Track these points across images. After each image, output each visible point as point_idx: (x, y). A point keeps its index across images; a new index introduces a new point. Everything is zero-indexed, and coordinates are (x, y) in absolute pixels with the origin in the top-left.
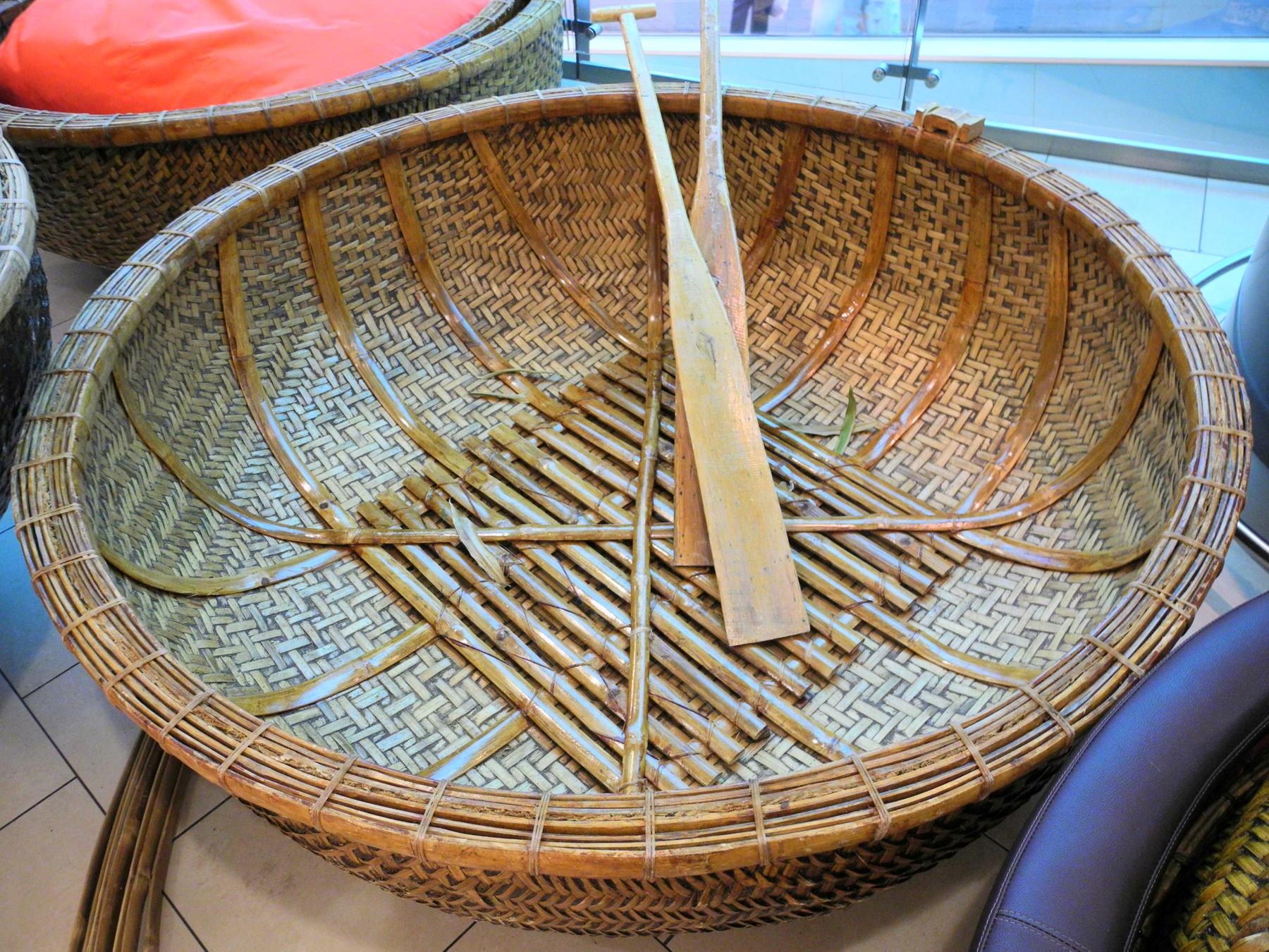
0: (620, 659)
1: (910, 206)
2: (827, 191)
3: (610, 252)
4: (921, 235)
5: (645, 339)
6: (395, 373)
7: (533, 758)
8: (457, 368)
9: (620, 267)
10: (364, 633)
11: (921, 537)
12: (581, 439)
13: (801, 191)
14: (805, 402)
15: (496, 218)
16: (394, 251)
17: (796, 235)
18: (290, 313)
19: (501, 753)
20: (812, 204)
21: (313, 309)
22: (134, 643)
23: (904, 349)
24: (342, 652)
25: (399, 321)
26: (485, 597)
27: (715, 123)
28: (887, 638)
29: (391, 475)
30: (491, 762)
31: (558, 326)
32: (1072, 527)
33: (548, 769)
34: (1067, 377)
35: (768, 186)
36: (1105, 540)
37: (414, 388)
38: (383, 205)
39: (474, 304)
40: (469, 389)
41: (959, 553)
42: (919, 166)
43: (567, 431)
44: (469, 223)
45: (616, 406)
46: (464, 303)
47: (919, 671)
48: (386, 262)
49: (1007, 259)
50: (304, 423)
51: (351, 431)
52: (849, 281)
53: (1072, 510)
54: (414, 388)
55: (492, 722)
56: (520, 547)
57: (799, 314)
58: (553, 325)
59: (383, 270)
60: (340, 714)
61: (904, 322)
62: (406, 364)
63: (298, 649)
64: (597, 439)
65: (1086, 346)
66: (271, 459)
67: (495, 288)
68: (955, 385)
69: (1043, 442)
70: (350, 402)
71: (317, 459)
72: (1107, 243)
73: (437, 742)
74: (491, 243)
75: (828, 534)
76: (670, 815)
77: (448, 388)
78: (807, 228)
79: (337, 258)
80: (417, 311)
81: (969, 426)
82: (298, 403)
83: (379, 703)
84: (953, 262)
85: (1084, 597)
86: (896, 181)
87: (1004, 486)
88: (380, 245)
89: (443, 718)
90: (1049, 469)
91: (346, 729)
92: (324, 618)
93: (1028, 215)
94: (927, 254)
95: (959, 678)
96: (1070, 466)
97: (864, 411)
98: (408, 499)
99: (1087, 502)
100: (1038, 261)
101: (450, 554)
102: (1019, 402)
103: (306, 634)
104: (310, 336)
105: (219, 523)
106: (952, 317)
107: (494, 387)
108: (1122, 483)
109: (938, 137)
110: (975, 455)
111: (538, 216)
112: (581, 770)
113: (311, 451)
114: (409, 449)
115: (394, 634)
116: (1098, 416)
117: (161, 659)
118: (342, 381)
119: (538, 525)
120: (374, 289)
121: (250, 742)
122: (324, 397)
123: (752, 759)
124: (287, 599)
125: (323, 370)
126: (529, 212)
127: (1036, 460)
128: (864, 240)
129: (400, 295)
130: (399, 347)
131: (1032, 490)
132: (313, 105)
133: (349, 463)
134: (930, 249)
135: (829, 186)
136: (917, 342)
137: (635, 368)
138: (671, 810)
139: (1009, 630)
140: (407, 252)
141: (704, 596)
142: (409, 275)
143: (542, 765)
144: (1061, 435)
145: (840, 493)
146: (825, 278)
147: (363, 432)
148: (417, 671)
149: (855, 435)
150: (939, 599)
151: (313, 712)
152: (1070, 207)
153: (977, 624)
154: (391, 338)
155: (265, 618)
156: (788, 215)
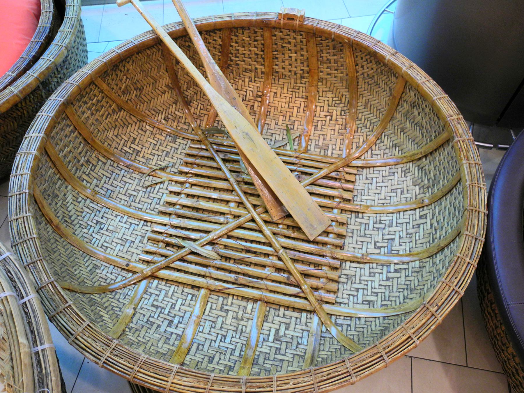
0: (280, 264)
1: (280, 47)
2: (243, 49)
3: (162, 102)
4: (287, 56)
5: (193, 132)
6: (108, 194)
8: (130, 178)
9: (168, 106)
11: (339, 170)
13: (232, 51)
14: (268, 134)
15: (112, 108)
16: (81, 143)
17: (234, 69)
18: (58, 193)
20: (238, 55)
21: (64, 186)
22: (199, 378)
24: (183, 317)
26: (216, 267)
27: (200, 40)
28: (352, 212)
31: (157, 142)
32: (387, 148)
33: (284, 315)
34: (361, 96)
35: (218, 53)
36: (402, 150)
37: (120, 196)
38: (70, 126)
40: (141, 185)
42: (281, 32)
43: (192, 185)
44: (103, 115)
45: (202, 166)
47: (368, 218)
48: (80, 149)
49: (325, 59)
50: (91, 235)
51: (110, 228)
52: (261, 80)
53: (384, 142)
54: (120, 196)
56: (216, 242)
57: (247, 99)
58: (155, 142)
59: (80, 153)
60: (204, 340)
61: (289, 90)
63: (168, 326)
64: (209, 183)
65: (367, 84)
66: (92, 258)
67: (123, 136)
68: (318, 108)
69: (361, 120)
70: (101, 215)
71: (107, 247)
72: (375, 52)
73: (242, 328)
74: (113, 120)
75: (312, 184)
76: (413, 328)
77: (133, 189)
78: (238, 65)
79: (62, 159)
80: (100, 163)
81: (331, 122)
82: (83, 229)
83: (212, 327)
84: (302, 63)
85: (405, 173)
86: (272, 39)
87: (354, 140)
88: (75, 144)
89: (236, 318)
90: (368, 130)
92: (165, 309)
93: (333, 43)
94: (290, 62)
95: (382, 215)
96: (375, 127)
97: (291, 129)
100: (339, 57)
101: (191, 258)
102: (345, 108)
103: (165, 319)
104: (70, 198)
105: (99, 297)
106: (307, 83)
107: (149, 181)
108: (399, 130)
109: (291, 22)
111: (128, 99)
112: (294, 309)
113: (102, 245)
115: (194, 299)
116: (380, 107)
117: (215, 378)
118: (92, 209)
119: (218, 230)
120: (81, 163)
121: (276, 386)
122: (90, 220)
123: (341, 274)
124: (146, 310)
125: (82, 209)
126: (124, 100)
127: (361, 128)
128: (263, 63)
129: (91, 160)
130: (103, 182)
132: (16, 95)
133: (120, 242)
134: (291, 60)
135: (244, 47)
136: (297, 96)
137: (199, 146)
138: (412, 326)
140: (85, 140)
141: (288, 226)
142: (90, 149)
143: (281, 314)
144: (367, 116)
145: (304, 166)
146: (251, 81)
147: (115, 226)
148: (214, 307)
149: (294, 140)
150: (358, 190)
152: (355, 40)
154: (98, 180)
156: (229, 62)
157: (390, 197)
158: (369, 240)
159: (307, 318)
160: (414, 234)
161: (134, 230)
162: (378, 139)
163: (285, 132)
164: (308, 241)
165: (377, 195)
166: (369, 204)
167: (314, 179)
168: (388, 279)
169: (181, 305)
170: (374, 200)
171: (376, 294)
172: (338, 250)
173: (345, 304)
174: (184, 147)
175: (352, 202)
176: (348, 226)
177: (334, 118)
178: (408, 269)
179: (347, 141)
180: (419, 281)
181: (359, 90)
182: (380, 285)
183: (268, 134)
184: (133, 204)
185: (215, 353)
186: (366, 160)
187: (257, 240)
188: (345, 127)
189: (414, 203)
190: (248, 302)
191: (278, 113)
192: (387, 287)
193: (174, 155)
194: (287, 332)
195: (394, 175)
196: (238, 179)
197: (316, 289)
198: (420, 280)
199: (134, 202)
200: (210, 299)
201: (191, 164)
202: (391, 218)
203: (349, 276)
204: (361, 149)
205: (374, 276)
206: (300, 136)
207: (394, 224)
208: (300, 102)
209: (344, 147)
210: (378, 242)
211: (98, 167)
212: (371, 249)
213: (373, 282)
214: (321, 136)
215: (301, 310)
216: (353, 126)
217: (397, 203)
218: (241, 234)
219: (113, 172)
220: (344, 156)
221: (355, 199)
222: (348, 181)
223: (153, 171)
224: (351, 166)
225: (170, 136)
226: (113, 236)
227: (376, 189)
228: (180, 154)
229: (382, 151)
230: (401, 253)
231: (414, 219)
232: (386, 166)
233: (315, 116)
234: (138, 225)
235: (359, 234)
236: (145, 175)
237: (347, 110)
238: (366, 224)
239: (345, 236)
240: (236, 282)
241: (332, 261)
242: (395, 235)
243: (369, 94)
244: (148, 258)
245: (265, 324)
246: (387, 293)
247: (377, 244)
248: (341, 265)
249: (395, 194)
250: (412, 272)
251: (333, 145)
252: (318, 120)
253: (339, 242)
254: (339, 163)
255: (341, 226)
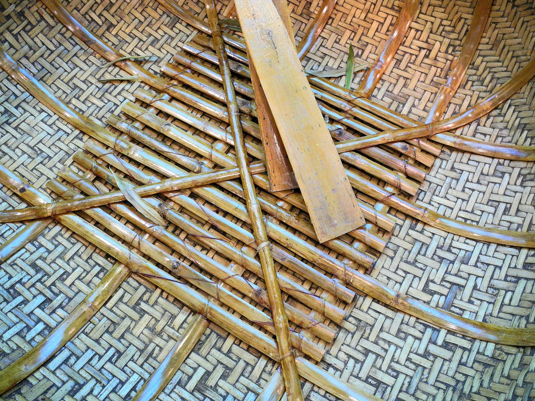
5: (206, 20)
6: (41, 74)
7: (218, 345)
10: (81, 280)
11: (411, 142)
12: (183, 103)
14: (319, 54)
19: (198, 346)
23: (376, 9)
24: (70, 299)
25: (32, 33)
28: (407, 216)
29: (62, 154)
30: (193, 355)
31: (146, 19)
32: (506, 128)
33: (230, 351)
37: (59, 83)
39: (83, 11)
40: (97, 76)
41: (436, 150)
46: (75, 12)
47: (431, 235)
51: (23, 126)
54: (59, 83)
55: (185, 325)
58: (142, 19)
60: (84, 348)
62: (48, 66)
63: (39, 307)
68: (413, 32)
69: (477, 69)
70: (15, 104)
73: (154, 349)
75: (358, 151)
77: (83, 78)
80: (43, 24)
81: (426, 61)
83: (107, 331)
87: (454, 100)
89: (152, 330)
90: (484, 88)
91: (91, 359)
92: (49, 276)
95: (456, 238)
96: (498, 85)
97: (357, 55)
98: (80, 170)
99: (514, 111)
102: (458, 42)
103: (41, 293)
107: (112, 74)
110: (432, 80)
114: (69, 131)
115: (101, 275)
116: (519, 53)
123: (350, 316)
124: (19, 269)
127: (473, 82)
129: (27, 13)
130: (38, 54)
131: (473, 102)
133: (29, 151)
137: (206, 44)
139: (479, 201)
141: (293, 208)
143: (225, 349)
144: (490, 65)
145: (356, 118)
147: (32, 125)
148: (125, 300)
149: (355, 74)
150: (430, 183)
151: (65, 353)
153: (458, 198)
154: (31, 48)
155: (8, 290)
157: (483, 212)
158: (419, 273)
159: (264, 371)
160: (502, 292)
161: (59, 139)
162: (496, 108)
163: (346, 57)
164: (316, 243)
165: (460, 200)
166: (441, 212)
167: (363, 144)
168: (426, 355)
169: (78, 278)
170: (452, 209)
171: (395, 374)
172: (361, 272)
173: (336, 369)
174: (184, 38)
175: (414, 200)
176: (393, 237)
177: (433, 54)
178: (470, 351)
179: (442, 97)
180: (481, 385)
181: (493, 14)
182: (408, 359)
183: (319, 54)
184: (74, 101)
185: (89, 377)
186: (463, 138)
187: (234, 213)
188: (447, 75)
189: (523, 236)
190: (181, 309)
191: (344, 25)
192: (420, 369)
193: (165, 45)
194: (221, 383)
195: (502, 177)
196: (243, 108)
197: (299, 327)
198: (486, 384)
199: (78, 99)
200: (125, 284)
201: (184, 66)
202: (470, 248)
203: (362, 324)
204: (460, 118)
205: (405, 339)
206: (368, 69)
207: (473, 261)
208: (385, 15)
209: (433, 107)
210: (433, 281)
211: (37, 30)
212: (417, 290)
213: (399, 350)
214: (401, 79)
215: (259, 354)
216: (460, 75)
217: (491, 226)
218: (214, 196)
219: (60, 44)
220: (427, 122)
221: (421, 197)
222: (419, 164)
223: (121, 61)
224: (433, 142)
225: (168, 16)
226: (22, 140)
227: (463, 191)
228: (174, 48)
229: (497, 130)
230: (466, 315)
231: (513, 265)
232: (493, 158)
233: (402, 44)
234: (68, 135)
235: (405, 256)
236: (109, 64)
237: (459, 45)
238: (423, 244)
239: (380, 253)
240: (174, 271)
241: (343, 289)
242: (467, 280)
243: (508, 24)
244: (63, 188)
245: (193, 355)
246: (416, 381)
247: (431, 284)
248: (355, 300)
249: (492, 210)
250: (475, 361)
251: (416, 98)
252: (406, 53)
253: (367, 259)
254: (414, 130)
255: (380, 235)
